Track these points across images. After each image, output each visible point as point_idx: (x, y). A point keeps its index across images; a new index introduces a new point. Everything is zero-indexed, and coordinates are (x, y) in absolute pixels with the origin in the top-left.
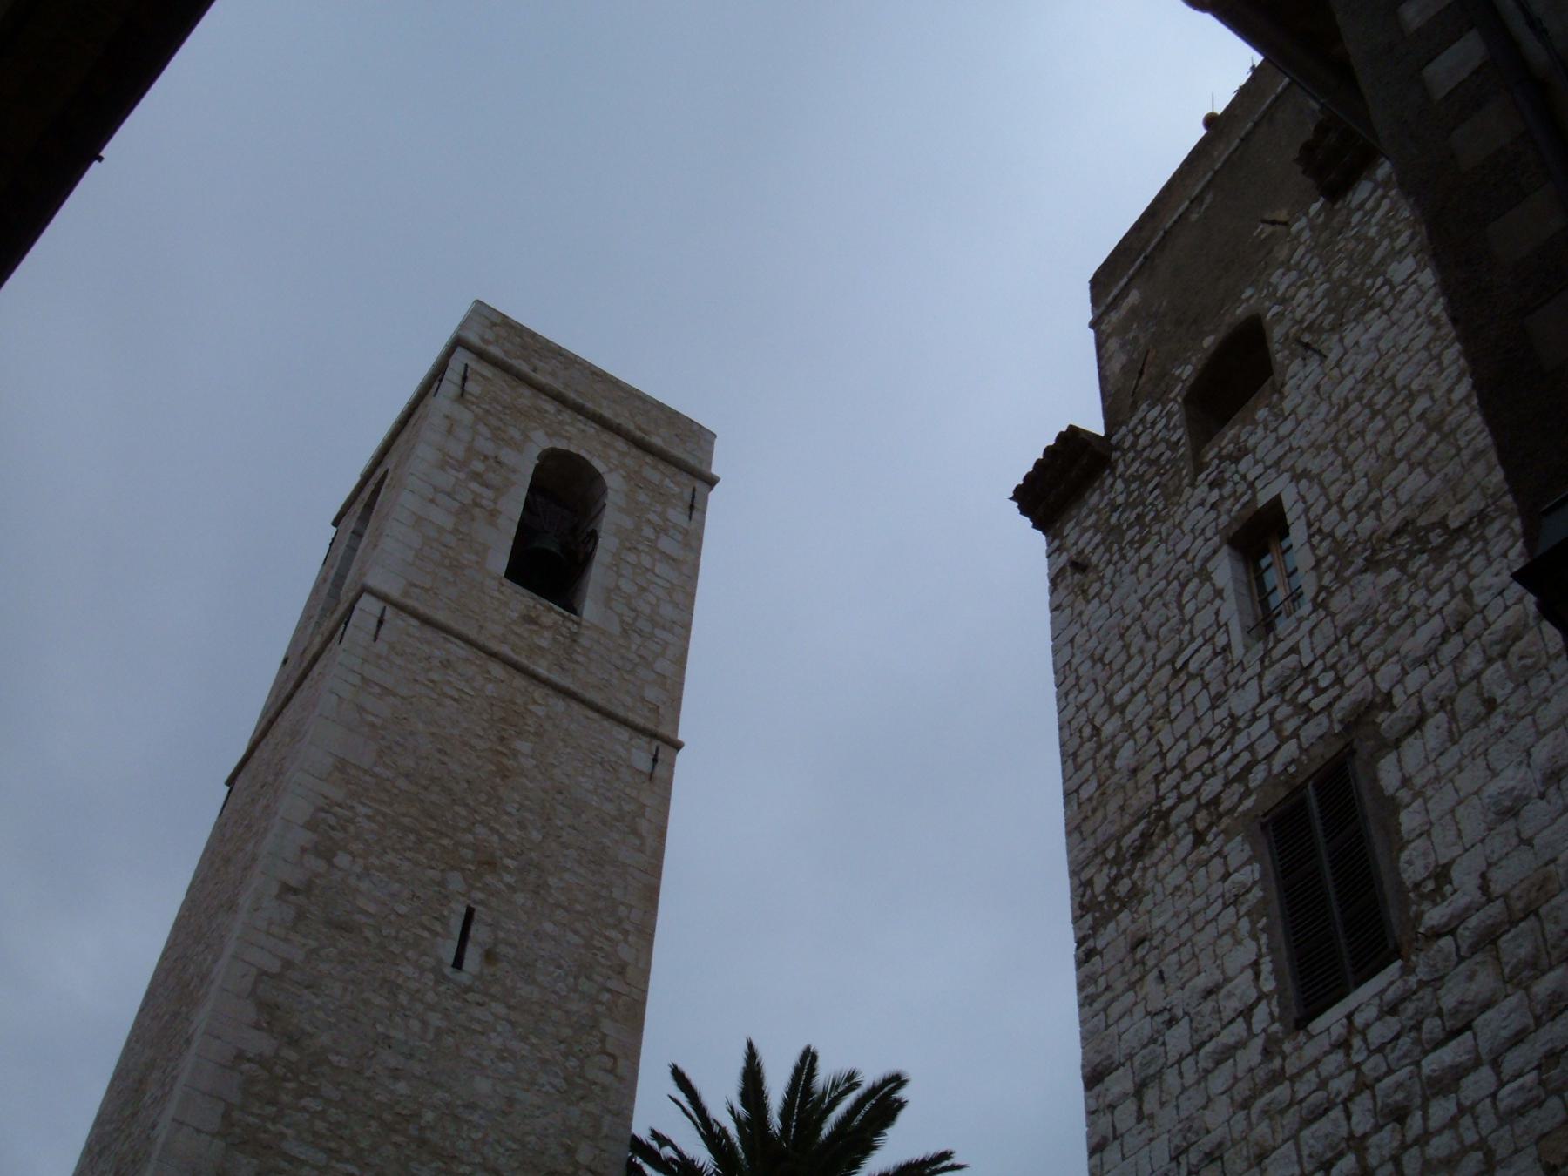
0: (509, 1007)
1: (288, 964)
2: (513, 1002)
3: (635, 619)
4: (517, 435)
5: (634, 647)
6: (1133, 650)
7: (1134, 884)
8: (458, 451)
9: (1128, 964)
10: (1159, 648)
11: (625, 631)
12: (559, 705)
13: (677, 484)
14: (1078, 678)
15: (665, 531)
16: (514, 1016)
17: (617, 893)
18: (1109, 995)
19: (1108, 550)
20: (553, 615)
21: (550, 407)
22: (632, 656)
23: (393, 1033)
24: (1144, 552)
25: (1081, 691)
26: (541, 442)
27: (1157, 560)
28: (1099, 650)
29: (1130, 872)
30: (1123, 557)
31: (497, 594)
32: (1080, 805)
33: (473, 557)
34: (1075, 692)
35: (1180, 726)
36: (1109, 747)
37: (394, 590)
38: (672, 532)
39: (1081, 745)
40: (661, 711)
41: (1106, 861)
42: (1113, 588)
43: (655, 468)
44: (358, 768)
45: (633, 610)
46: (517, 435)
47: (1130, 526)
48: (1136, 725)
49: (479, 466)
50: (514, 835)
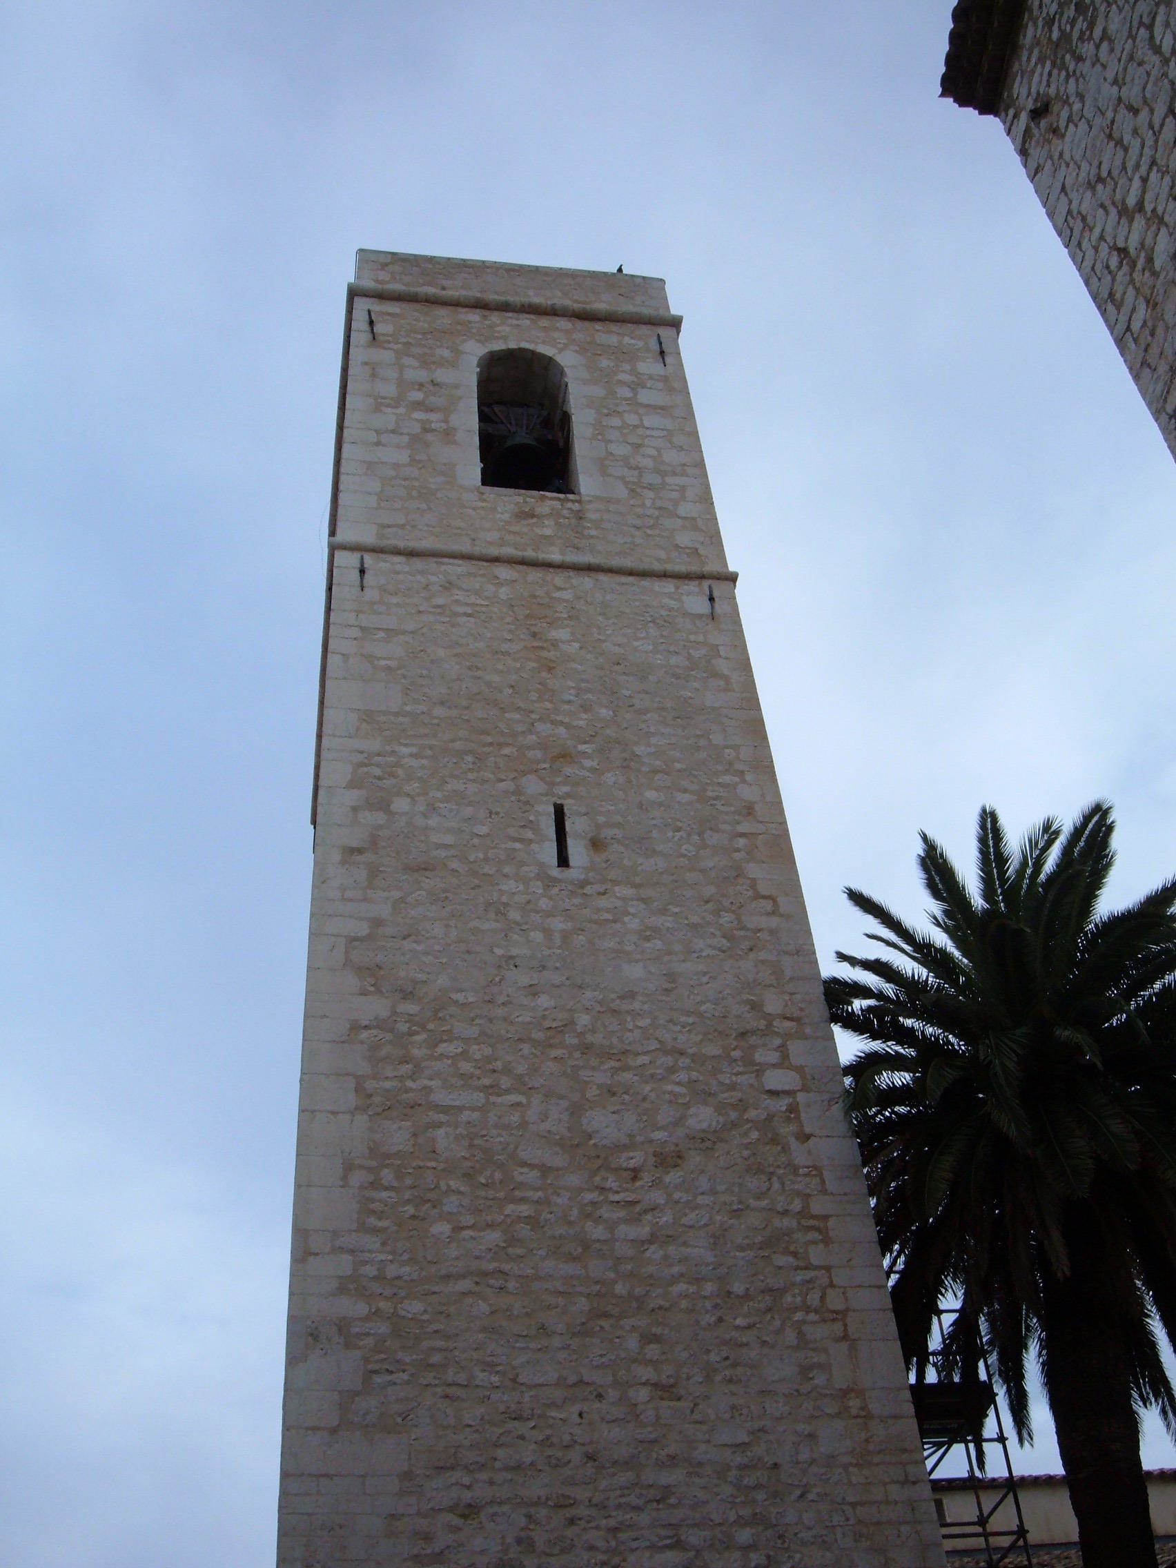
0: (635, 886)
1: (377, 923)
2: (637, 880)
5: (648, 503)
6: (1127, 138)
8: (390, 390)
10: (1152, 111)
14: (1084, 219)
16: (644, 893)
17: (717, 739)
24: (1097, 33)
25: (1091, 230)
26: (474, 352)
27: (1113, 27)
28: (1094, 171)
32: (1135, 340)
36: (1143, 254)
39: (1113, 280)
47: (1073, 23)
48: (1160, 210)
50: (582, 721)
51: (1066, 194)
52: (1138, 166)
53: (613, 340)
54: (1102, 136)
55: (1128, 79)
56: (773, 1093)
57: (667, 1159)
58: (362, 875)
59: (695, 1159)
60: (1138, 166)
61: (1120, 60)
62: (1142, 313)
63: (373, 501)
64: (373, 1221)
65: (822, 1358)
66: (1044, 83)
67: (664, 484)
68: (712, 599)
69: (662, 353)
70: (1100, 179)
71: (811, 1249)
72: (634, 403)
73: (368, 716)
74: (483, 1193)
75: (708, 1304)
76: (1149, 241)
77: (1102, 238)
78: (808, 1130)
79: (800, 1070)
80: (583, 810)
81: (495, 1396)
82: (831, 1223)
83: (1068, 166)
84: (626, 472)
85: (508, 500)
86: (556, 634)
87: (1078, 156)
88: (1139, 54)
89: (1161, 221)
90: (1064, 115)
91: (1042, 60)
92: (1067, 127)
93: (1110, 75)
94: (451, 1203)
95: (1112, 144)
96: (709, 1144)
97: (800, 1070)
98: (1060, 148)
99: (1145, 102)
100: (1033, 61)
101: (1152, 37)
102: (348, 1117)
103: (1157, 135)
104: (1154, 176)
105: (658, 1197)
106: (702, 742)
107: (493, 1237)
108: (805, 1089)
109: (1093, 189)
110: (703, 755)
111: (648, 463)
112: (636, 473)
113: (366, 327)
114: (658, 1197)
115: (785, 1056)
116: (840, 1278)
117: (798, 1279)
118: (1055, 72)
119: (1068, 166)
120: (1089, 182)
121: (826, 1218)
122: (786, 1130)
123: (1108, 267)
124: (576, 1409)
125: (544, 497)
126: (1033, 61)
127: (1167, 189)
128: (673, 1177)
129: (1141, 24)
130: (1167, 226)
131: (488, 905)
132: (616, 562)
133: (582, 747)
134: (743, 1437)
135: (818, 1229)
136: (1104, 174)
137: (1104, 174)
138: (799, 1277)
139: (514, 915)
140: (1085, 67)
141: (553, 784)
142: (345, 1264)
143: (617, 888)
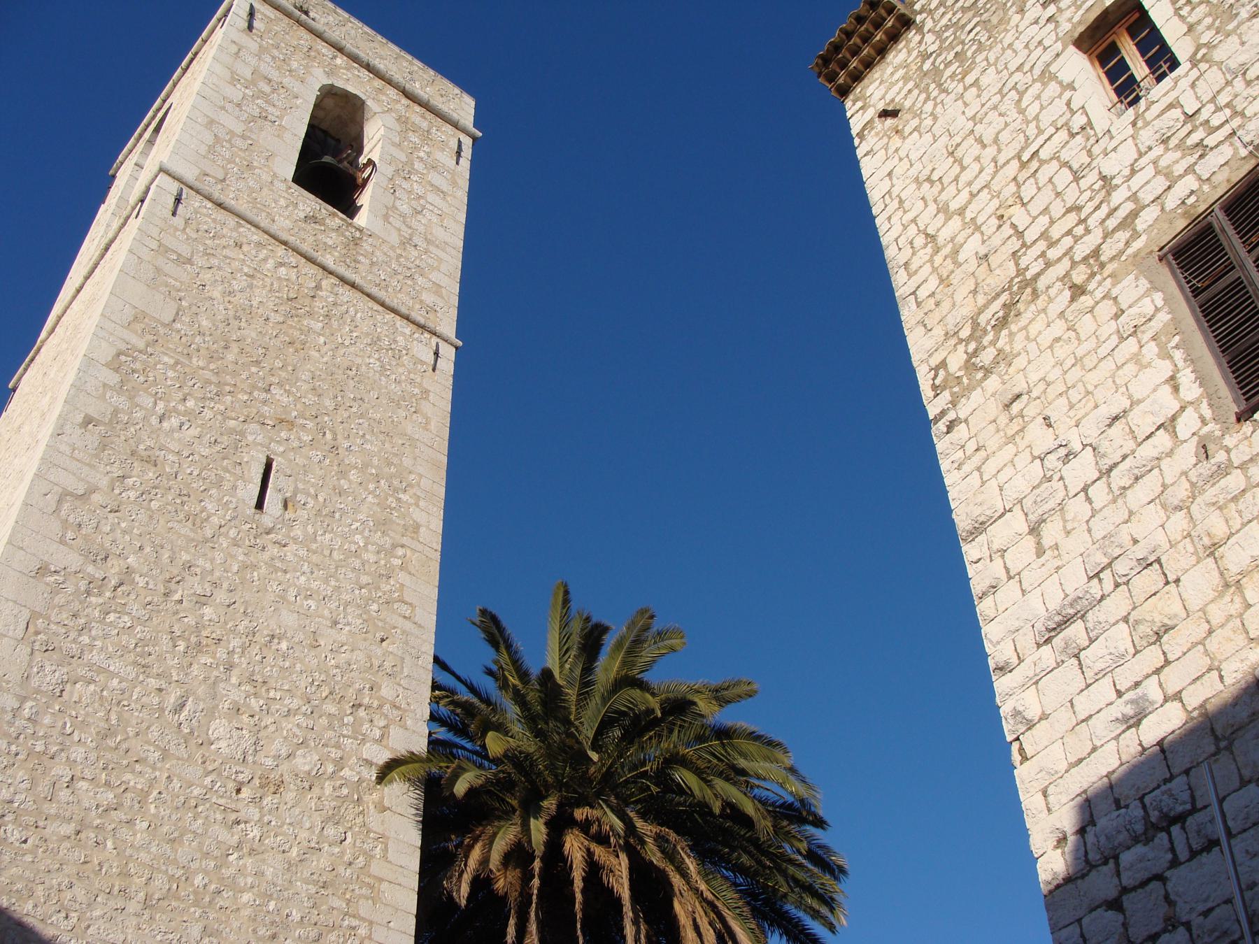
7: (1000, 351)
9: (1003, 420)
10: (999, 151)
12: (346, 294)
14: (901, 202)
17: (407, 462)
18: (982, 453)
23: (201, 562)
24: (970, 79)
25: (905, 212)
26: (319, 79)
27: (984, 81)
28: (926, 172)
29: (993, 343)
30: (946, 91)
32: (918, 304)
35: (1035, 208)
36: (950, 245)
42: (935, 118)
43: (423, 117)
48: (980, 221)
51: (891, 179)
52: (970, 184)
53: (425, 125)
54: (945, 151)
60: (970, 184)
61: (983, 105)
62: (933, 283)
63: (203, 150)
70: (929, 179)
76: (960, 239)
77: (914, 221)
78: (386, 804)
82: (385, 886)
83: (901, 159)
84: (403, 228)
85: (309, 203)
88: (1002, 108)
89: (978, 228)
90: (915, 122)
91: (906, 79)
92: (911, 133)
93: (969, 113)
99: (996, 140)
100: (897, 76)
101: (1019, 101)
102: (13, 642)
105: (254, 813)
106: (395, 460)
110: (393, 470)
111: (422, 229)
112: (410, 231)
118: (916, 92)
119: (901, 159)
120: (917, 179)
121: (381, 880)
123: (911, 243)
125: (334, 215)
126: (897, 76)
129: (1014, 87)
130: (982, 233)
135: (372, 887)
136: (935, 177)
137: (935, 177)
140: (949, 100)
141: (272, 440)
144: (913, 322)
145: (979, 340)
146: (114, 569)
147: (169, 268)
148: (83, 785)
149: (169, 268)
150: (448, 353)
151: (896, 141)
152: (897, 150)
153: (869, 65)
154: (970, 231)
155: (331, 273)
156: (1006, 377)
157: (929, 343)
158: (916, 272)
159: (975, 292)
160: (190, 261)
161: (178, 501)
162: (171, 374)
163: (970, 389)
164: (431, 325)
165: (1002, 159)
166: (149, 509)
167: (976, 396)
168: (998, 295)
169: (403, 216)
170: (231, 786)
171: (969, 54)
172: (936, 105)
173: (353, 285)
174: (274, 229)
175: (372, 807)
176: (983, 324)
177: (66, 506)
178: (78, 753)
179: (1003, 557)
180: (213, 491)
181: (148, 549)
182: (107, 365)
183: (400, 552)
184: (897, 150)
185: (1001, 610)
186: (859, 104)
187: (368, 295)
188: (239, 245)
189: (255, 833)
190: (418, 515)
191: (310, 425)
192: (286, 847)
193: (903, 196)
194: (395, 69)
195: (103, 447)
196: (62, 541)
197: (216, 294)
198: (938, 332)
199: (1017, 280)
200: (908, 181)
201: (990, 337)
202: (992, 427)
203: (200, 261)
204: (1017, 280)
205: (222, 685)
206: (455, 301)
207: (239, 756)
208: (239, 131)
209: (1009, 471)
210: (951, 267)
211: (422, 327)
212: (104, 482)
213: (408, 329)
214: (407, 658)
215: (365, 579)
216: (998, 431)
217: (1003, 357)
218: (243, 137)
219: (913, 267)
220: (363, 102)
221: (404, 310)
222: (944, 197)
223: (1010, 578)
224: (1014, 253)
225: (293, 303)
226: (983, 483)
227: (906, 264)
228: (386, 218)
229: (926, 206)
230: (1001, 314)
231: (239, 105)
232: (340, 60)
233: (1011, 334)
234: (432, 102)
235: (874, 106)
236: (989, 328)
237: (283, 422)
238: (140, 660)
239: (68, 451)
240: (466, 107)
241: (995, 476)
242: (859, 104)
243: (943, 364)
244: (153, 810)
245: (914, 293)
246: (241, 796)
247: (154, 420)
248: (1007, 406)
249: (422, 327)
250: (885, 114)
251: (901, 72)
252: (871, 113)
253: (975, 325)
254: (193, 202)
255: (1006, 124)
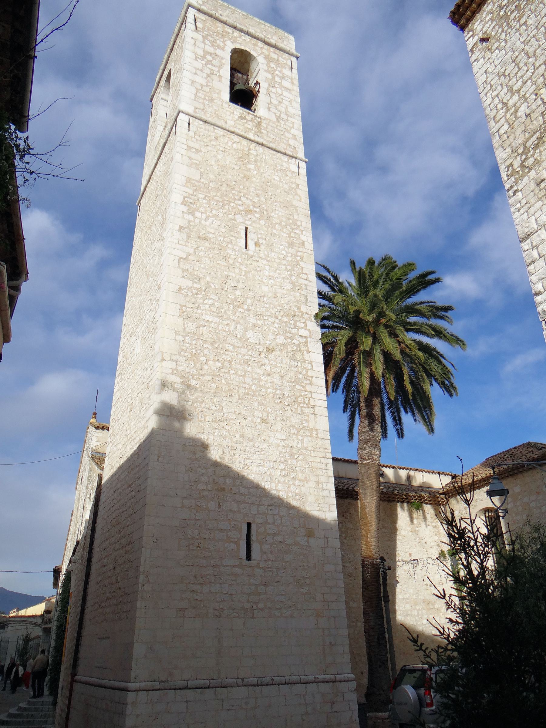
0: (268, 261)
1: (189, 254)
2: (268, 259)
3: (280, 114)
4: (222, 45)
5: (282, 125)
6: (521, 65)
7: (536, 159)
8: (200, 52)
9: (537, 191)
10: (536, 60)
11: (277, 119)
12: (260, 149)
13: (284, 58)
14: (491, 86)
15: (283, 78)
16: (270, 264)
17: (296, 217)
18: (528, 205)
19: (501, 26)
20: (250, 116)
21: (230, 30)
22: (282, 129)
23: (231, 274)
24: (522, 21)
25: (493, 91)
26: (230, 46)
27: (530, 22)
28: (502, 71)
29: (533, 156)
30: (511, 27)
31: (228, 109)
32: (500, 137)
33: (216, 95)
34: (491, 92)
36: (514, 108)
37: (191, 111)
38: (286, 78)
39: (497, 112)
40: (297, 149)
41: (519, 154)
42: (506, 42)
43: (275, 53)
44: (195, 180)
45: (279, 111)
46: (222, 45)
47: (512, 12)
48: (527, 96)
49: (209, 58)
50: (256, 199)
53: (276, 57)
54: (510, 60)
55: (530, 44)
56: (301, 336)
57: (270, 350)
58: (185, 236)
59: (277, 353)
60: (522, 77)
61: (529, 35)
62: (506, 127)
64: (182, 353)
65: (306, 418)
66: (491, 28)
67: (287, 120)
68: (299, 167)
69: (292, 67)
70: (503, 74)
71: (307, 385)
72: (280, 84)
73: (188, 180)
74: (216, 351)
75: (278, 397)
77: (497, 96)
79: (309, 331)
80: (254, 231)
81: (216, 413)
82: (314, 379)
83: (491, 64)
84: (276, 111)
85: (238, 110)
86: (249, 166)
87: (497, 62)
89: (526, 100)
90: (496, 44)
92: (495, 50)
93: (522, 40)
94: (206, 352)
95: (513, 64)
96: (282, 348)
97: (309, 331)
98: (489, 56)
99: (534, 55)
100: (488, 18)
103: (535, 69)
104: (529, 83)
105: (267, 361)
106: (291, 217)
107: (219, 364)
108: (310, 337)
109: (499, 77)
110: (291, 221)
113: (193, 22)
114: (267, 361)
115: (305, 325)
116: (314, 395)
117: (303, 394)
119: (491, 64)
120: (498, 74)
121: (312, 377)
122: (304, 348)
123: (496, 107)
124: (238, 421)
125: (249, 113)
126: (488, 18)
127: (533, 90)
128: (271, 356)
131: (223, 257)
132: (271, 145)
133: (255, 209)
134: (284, 437)
136: (506, 74)
137: (507, 74)
138: (303, 393)
139: (231, 262)
141: (246, 220)
142: (173, 365)
143: (262, 261)
144: (497, 145)
145: (526, 154)
146: (203, 282)
147: (193, 155)
148: (210, 362)
149: (193, 155)
150: (303, 165)
151: (488, 54)
152: (489, 59)
153: (474, 13)
154: (523, 101)
155: (253, 141)
156: (538, 171)
157: (505, 156)
158: (498, 121)
159: (524, 131)
160: (200, 151)
161: (219, 252)
162: (204, 201)
163: (523, 176)
164: (294, 155)
165: (537, 65)
166: (209, 258)
167: (525, 179)
168: (535, 133)
169: (276, 106)
170: (258, 353)
171: (522, 6)
172: (506, 35)
173: (262, 145)
174: (227, 127)
175: (305, 352)
176: (528, 147)
177: (181, 263)
178: (206, 352)
179: (537, 248)
180: (230, 246)
181: (213, 273)
182: (182, 204)
183: (299, 254)
184: (489, 59)
185: (537, 270)
186: (471, 33)
187: (269, 148)
188: (216, 138)
189: (268, 368)
190: (303, 238)
191: (258, 210)
192: (279, 371)
193: (492, 83)
194: (259, 31)
195: (188, 237)
196: (183, 277)
197: (213, 163)
198: (509, 150)
199: (543, 126)
200: (494, 76)
201: (531, 153)
202: (532, 194)
203: (204, 150)
204: (543, 126)
205: (247, 318)
206: (302, 140)
207: (258, 342)
208: (204, 83)
209: (539, 213)
210: (514, 119)
211: (292, 157)
212: (192, 251)
213: (286, 158)
214: (308, 295)
215: (289, 268)
216: (535, 195)
217: (537, 162)
218: (207, 86)
219: (498, 118)
220: (249, 53)
221: (283, 151)
222: (510, 84)
223: (540, 257)
224: (542, 113)
225: (243, 158)
226: (529, 218)
227: (494, 118)
228: (269, 109)
229: (503, 88)
230: (536, 142)
231: (201, 70)
232: (237, 33)
233: (541, 152)
234: (277, 44)
235: (478, 35)
236: (531, 149)
237: (248, 211)
238: (219, 315)
239: (176, 241)
240: (291, 42)
241: (534, 215)
242: (471, 33)
243: (511, 165)
244: (234, 367)
245: (498, 131)
246: (261, 356)
247: (203, 222)
248: (538, 185)
249: (292, 157)
250: (483, 40)
251: (490, 16)
252: (476, 38)
253: (525, 147)
254: (195, 123)
255: (540, 46)
